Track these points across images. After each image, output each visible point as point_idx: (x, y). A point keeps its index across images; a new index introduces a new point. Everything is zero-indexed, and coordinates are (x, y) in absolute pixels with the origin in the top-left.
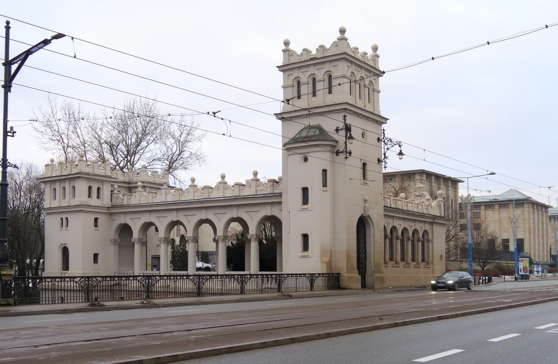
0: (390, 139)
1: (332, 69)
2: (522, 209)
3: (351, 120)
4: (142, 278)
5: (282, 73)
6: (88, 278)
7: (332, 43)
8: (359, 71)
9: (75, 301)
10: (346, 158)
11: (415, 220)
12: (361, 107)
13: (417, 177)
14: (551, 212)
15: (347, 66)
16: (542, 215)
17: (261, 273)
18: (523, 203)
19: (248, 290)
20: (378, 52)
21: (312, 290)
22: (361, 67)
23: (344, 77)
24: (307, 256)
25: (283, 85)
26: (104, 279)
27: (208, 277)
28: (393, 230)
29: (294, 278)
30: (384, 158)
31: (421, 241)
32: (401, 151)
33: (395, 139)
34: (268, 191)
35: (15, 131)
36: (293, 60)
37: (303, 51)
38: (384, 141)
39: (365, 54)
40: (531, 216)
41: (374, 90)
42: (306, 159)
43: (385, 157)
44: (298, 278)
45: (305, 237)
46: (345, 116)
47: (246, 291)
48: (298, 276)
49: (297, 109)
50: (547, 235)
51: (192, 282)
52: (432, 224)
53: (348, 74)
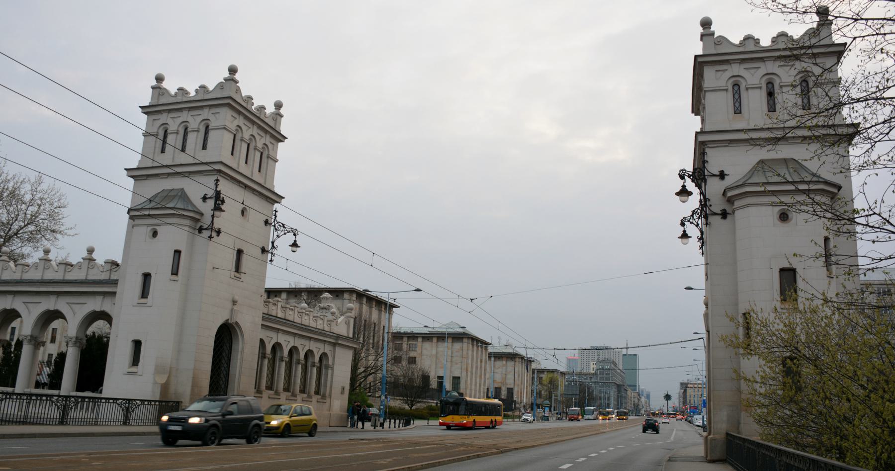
0: (283, 224)
1: (211, 117)
2: (461, 344)
3: (226, 188)
4: (122, 402)
6: (129, 400)
7: (217, 84)
8: (234, 117)
9: (51, 423)
10: (210, 237)
11: (310, 338)
12: (233, 167)
13: (346, 296)
14: (490, 349)
15: (232, 116)
16: (482, 353)
17: (74, 394)
18: (463, 338)
19: (53, 418)
20: (282, 111)
21: (126, 425)
22: (253, 123)
23: (225, 128)
24: (135, 373)
26: (107, 401)
27: (80, 400)
28: (277, 347)
29: (110, 404)
30: (272, 248)
31: (286, 361)
32: (295, 241)
33: (289, 224)
34: (103, 277)
35: (95, 258)
36: (163, 100)
38: (274, 226)
39: (262, 107)
40: (470, 352)
41: (268, 157)
42: (155, 234)
43: (273, 247)
44: (102, 404)
45: (137, 344)
46: (217, 180)
47: (70, 421)
48: (146, 403)
49: (156, 164)
50: (485, 375)
51: (119, 408)
52: (334, 345)
53: (233, 127)
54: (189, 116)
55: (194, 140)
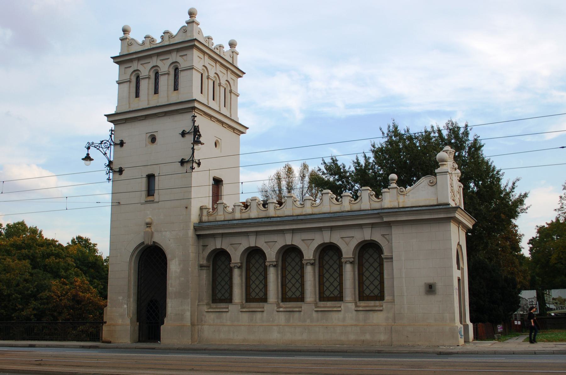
1: (179, 60)
5: (118, 66)
10: (374, 146)
25: (117, 80)
37: (145, 38)
54: (159, 61)
55: (165, 82)
